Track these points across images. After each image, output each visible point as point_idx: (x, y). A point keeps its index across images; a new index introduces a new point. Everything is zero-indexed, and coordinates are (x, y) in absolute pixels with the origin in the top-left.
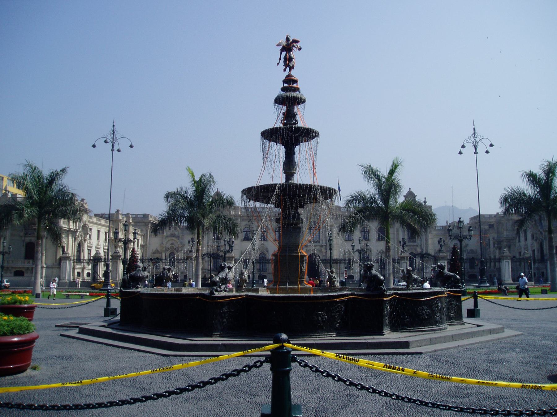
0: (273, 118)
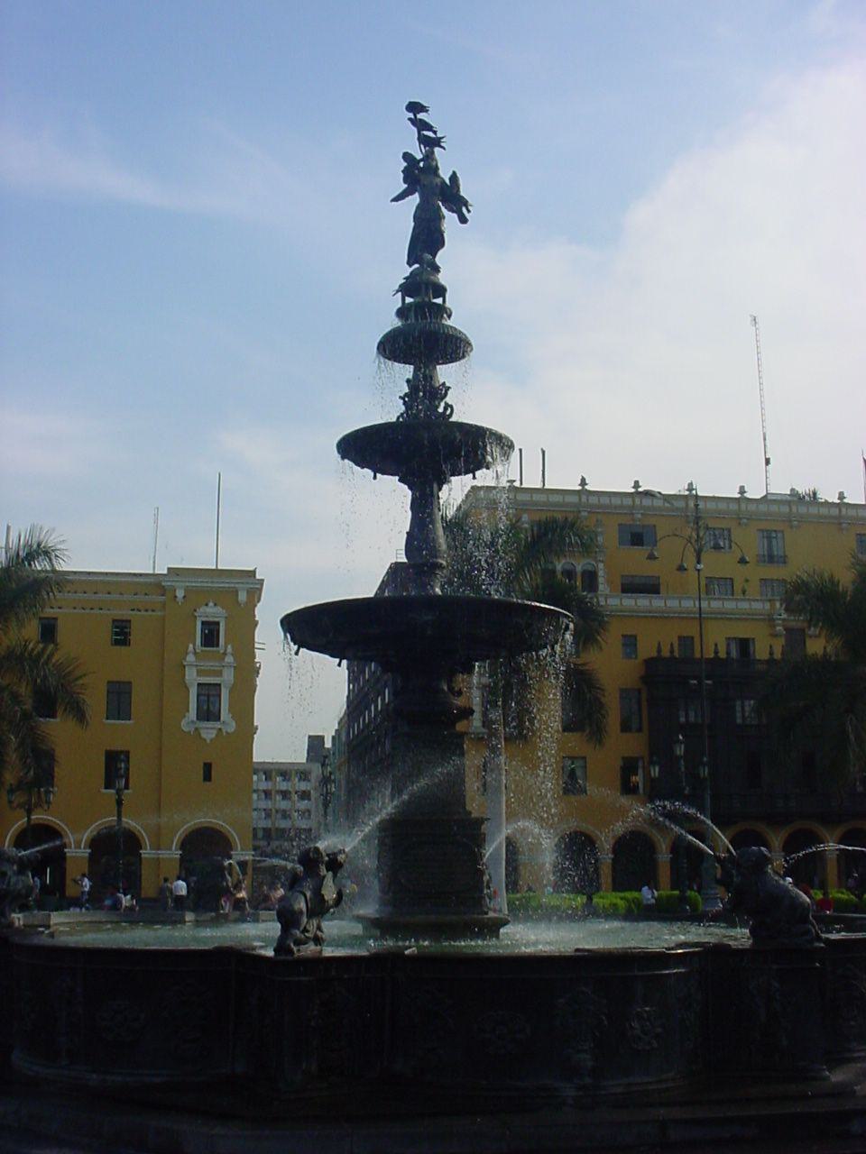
0: (381, 398)
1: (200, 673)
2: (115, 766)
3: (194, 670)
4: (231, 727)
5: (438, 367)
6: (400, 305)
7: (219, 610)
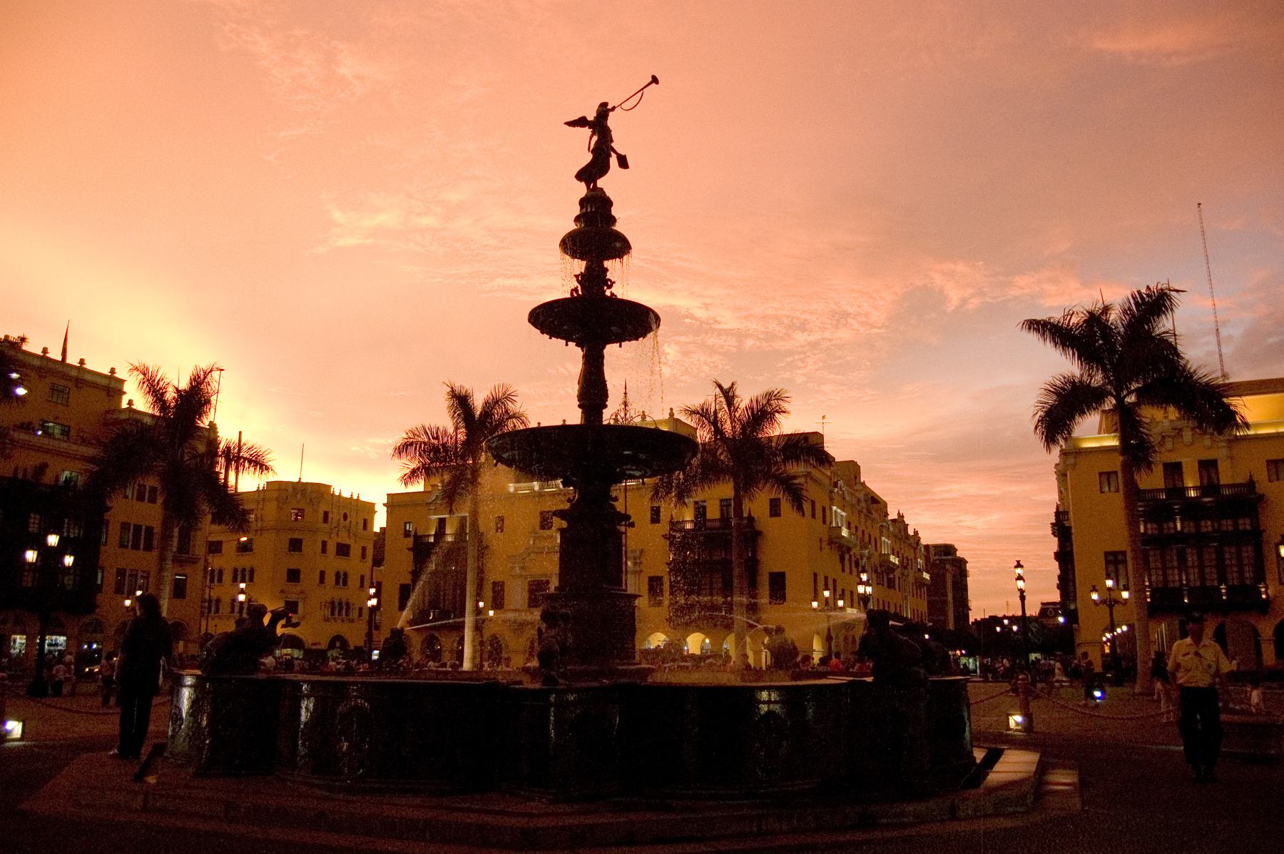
0: (559, 279)
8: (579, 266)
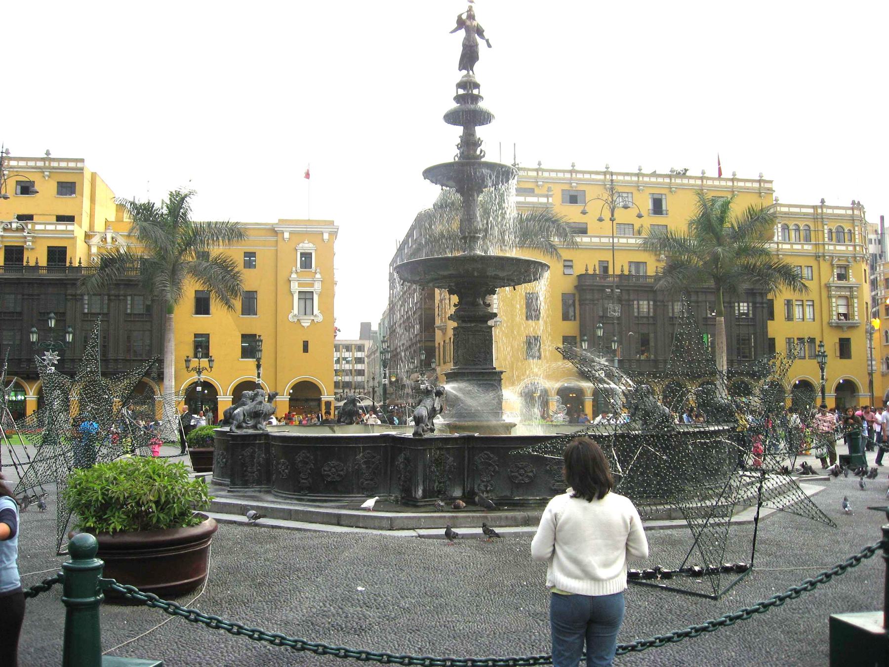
0: (446, 146)
1: (300, 285)
2: (251, 347)
3: (297, 283)
4: (320, 318)
5: (477, 128)
6: (455, 95)
7: (311, 245)
8: (459, 130)
